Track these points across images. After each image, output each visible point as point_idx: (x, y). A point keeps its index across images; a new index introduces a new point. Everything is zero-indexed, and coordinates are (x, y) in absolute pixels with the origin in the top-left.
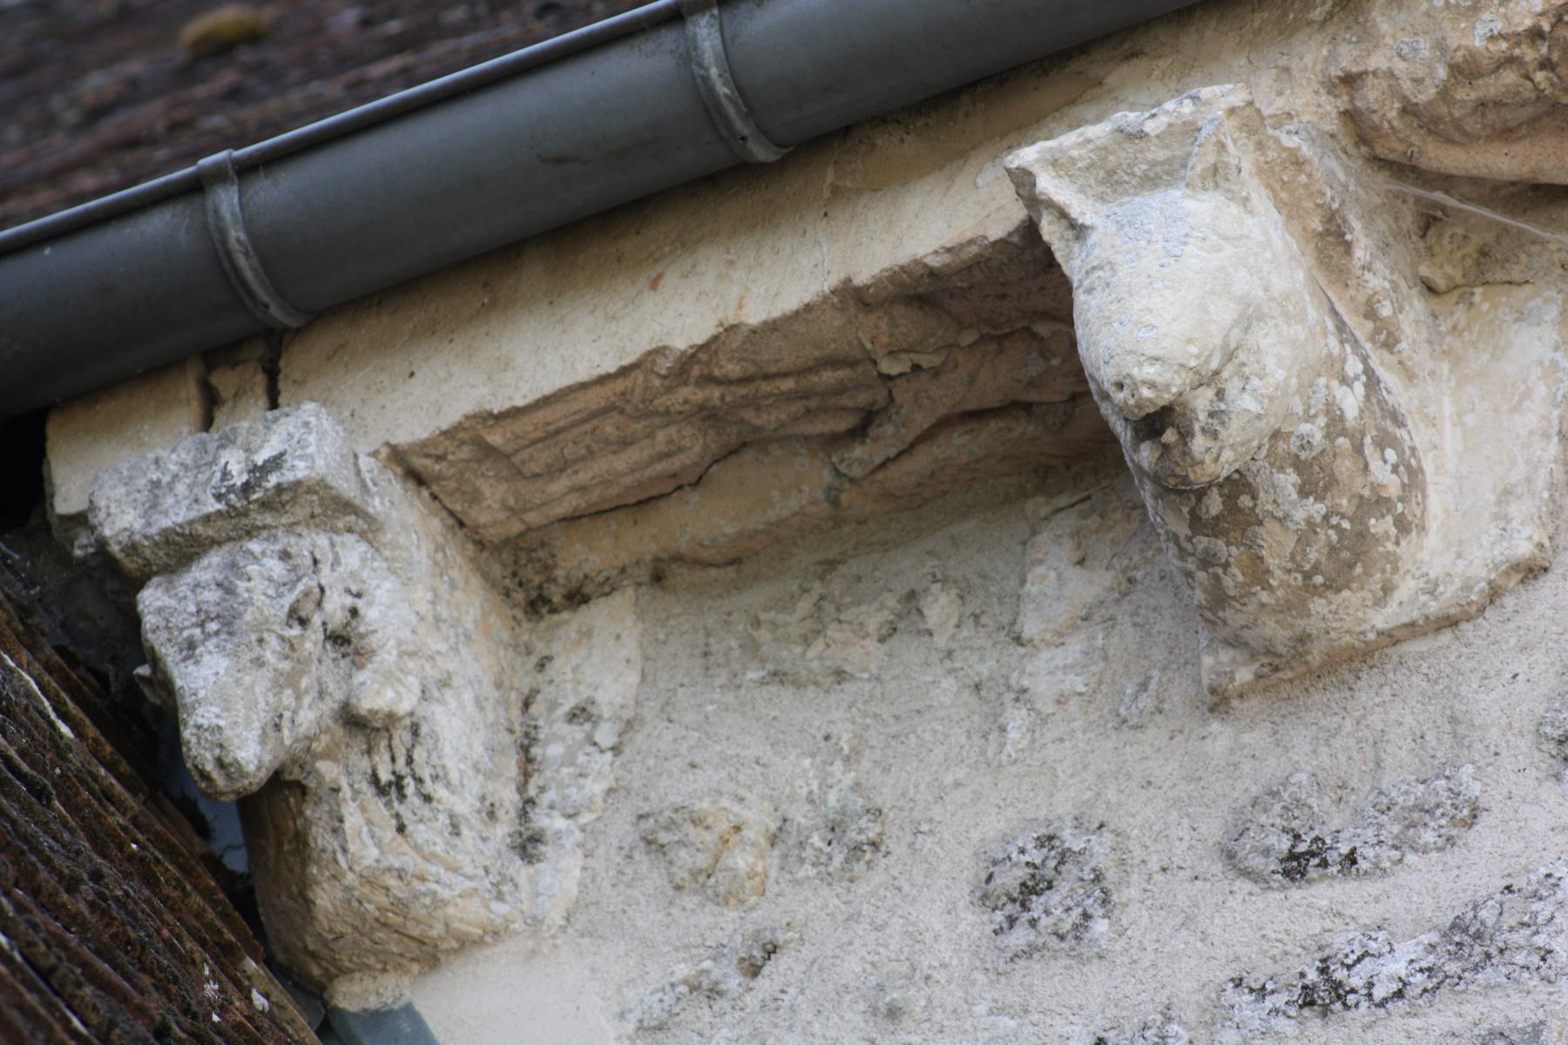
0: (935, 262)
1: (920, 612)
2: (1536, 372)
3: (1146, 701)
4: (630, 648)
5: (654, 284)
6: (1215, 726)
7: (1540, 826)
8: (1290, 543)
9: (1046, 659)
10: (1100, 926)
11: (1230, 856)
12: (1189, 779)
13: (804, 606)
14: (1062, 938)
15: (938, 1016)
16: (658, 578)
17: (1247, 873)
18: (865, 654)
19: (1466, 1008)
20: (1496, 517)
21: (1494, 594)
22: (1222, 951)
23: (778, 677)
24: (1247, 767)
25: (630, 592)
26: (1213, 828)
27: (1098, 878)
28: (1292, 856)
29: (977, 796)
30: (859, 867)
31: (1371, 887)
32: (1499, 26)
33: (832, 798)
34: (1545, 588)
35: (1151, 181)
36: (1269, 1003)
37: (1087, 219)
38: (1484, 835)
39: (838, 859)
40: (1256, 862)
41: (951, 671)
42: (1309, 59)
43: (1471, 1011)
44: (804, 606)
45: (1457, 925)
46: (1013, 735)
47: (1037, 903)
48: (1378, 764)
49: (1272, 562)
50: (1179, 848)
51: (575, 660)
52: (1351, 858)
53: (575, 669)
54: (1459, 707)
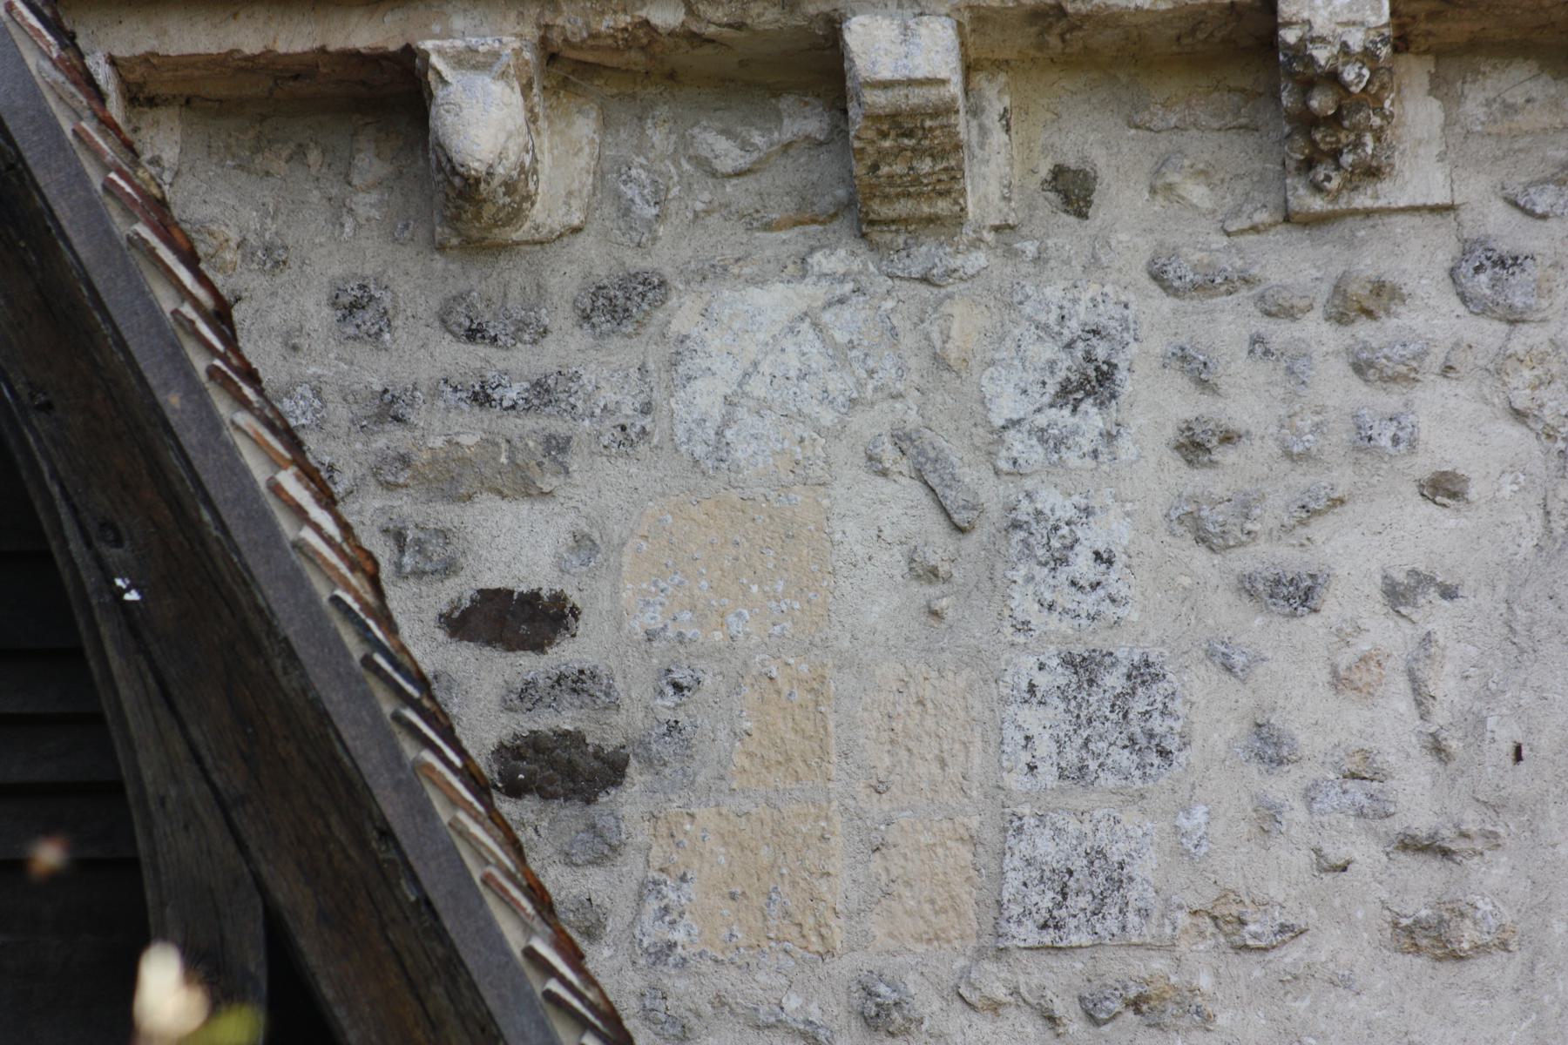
0: (363, 51)
1: (305, 155)
2: (585, 141)
3: (407, 234)
4: (177, 137)
5: (235, 16)
6: (437, 256)
7: (573, 347)
8: (494, 210)
9: (361, 198)
10: (387, 336)
11: (443, 321)
12: (425, 277)
13: (251, 133)
14: (370, 336)
15: (313, 354)
16: (188, 101)
17: (451, 332)
18: (279, 166)
19: (540, 421)
20: (565, 203)
21: (561, 236)
22: (439, 365)
23: (240, 167)
24: (451, 280)
25: (177, 108)
26: (435, 304)
27: (386, 312)
28: (470, 329)
29: (330, 253)
30: (277, 271)
31: (503, 354)
32: (612, 24)
33: (267, 236)
34: (581, 237)
35: (475, 67)
36: (459, 394)
37: (449, 79)
38: (550, 343)
39: (268, 265)
40: (456, 329)
41: (317, 188)
42: (532, 12)
43: (543, 422)
44: (251, 133)
45: (538, 383)
46: (347, 230)
47: (359, 314)
48: (505, 295)
49: (485, 215)
50: (421, 309)
51: (151, 134)
52: (495, 339)
53: (151, 138)
54: (542, 282)
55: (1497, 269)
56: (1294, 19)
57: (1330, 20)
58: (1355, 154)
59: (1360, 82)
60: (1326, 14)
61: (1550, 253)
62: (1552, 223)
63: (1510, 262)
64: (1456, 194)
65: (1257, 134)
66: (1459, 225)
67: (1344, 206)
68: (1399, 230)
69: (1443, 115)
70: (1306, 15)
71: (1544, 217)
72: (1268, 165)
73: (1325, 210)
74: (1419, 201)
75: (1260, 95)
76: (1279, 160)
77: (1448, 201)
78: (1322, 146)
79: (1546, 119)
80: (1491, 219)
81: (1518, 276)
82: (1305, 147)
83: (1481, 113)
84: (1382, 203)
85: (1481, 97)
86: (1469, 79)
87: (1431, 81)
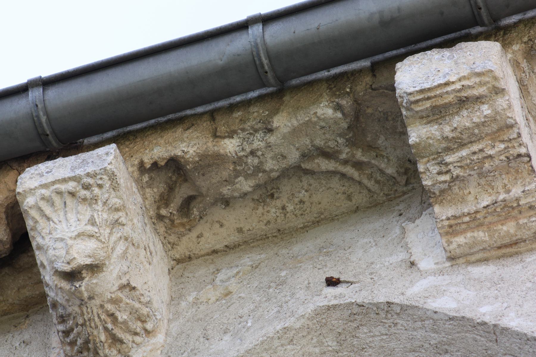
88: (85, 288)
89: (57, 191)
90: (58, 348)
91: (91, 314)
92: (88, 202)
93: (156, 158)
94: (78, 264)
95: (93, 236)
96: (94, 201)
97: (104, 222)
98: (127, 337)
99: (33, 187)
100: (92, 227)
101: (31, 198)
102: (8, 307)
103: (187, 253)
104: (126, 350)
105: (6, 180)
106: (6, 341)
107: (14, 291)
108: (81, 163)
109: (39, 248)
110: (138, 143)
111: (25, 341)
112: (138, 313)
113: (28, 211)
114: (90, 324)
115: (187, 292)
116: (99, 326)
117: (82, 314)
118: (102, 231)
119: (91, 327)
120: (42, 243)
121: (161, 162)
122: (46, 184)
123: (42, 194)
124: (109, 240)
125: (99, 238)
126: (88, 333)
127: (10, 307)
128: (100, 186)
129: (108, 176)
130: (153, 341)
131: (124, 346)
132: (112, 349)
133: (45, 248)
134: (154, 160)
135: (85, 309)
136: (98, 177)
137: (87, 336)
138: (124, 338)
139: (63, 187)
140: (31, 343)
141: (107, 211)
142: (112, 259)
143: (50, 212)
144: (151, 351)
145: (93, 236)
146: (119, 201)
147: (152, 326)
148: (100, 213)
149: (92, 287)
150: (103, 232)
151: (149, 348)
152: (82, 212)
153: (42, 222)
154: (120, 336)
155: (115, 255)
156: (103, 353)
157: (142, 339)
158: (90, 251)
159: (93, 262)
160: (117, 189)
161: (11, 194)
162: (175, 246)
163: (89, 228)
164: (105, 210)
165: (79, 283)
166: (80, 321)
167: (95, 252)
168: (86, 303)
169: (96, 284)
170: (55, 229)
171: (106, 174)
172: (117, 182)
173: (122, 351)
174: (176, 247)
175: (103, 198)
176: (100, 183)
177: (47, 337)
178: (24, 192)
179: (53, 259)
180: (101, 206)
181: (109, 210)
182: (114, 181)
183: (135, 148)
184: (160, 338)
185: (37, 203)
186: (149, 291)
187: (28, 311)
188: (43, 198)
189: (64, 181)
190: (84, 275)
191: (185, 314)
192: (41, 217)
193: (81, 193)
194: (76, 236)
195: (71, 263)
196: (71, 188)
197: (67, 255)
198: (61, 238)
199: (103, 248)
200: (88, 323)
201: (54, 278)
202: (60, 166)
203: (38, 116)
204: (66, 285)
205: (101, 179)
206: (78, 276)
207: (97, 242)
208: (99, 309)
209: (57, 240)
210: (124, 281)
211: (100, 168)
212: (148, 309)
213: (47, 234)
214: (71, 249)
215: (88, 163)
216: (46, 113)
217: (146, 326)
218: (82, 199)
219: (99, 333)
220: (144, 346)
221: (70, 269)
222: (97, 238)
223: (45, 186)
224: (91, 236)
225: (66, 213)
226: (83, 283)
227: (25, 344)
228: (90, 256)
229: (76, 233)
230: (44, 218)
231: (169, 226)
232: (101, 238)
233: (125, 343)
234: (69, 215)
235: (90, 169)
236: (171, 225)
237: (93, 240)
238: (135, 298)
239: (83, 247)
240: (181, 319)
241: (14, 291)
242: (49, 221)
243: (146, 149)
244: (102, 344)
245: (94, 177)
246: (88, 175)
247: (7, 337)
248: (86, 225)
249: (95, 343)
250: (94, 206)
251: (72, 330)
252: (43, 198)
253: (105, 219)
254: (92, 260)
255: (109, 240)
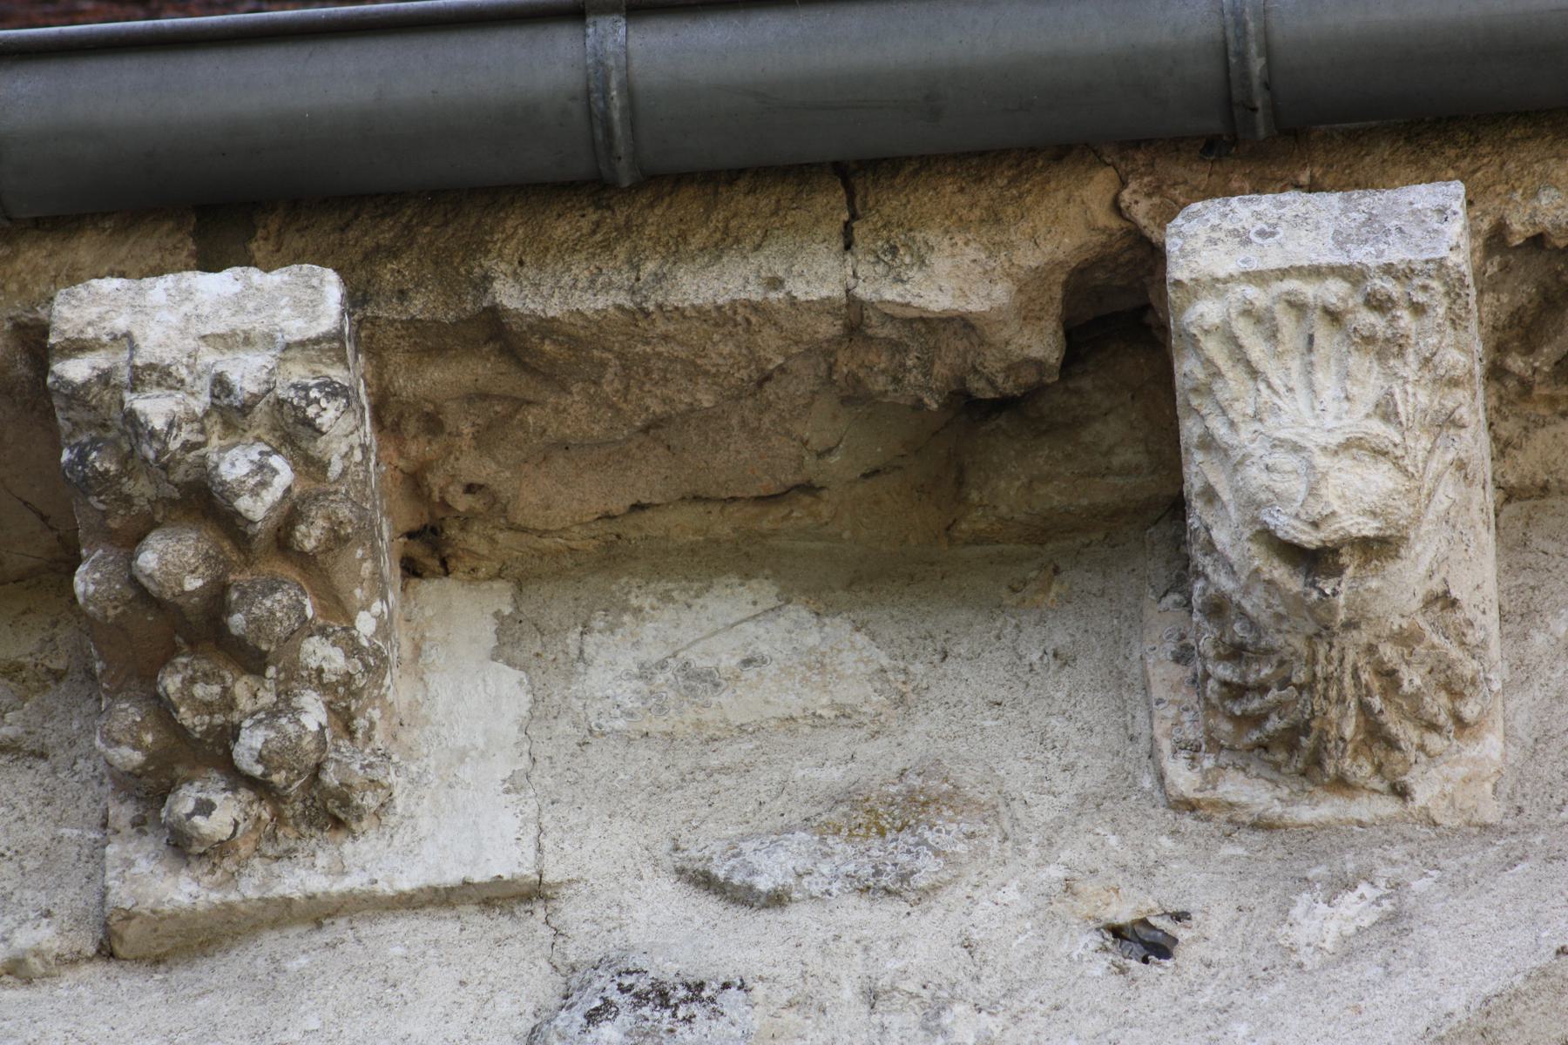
55: (646, 1011)
56: (90, 333)
57: (183, 332)
58: (270, 727)
59: (264, 484)
60: (174, 319)
61: (788, 975)
62: (798, 915)
63: (682, 993)
64: (550, 860)
65: (43, 766)
66: (557, 933)
67: (252, 894)
68: (398, 951)
69: (526, 699)
70: (121, 323)
71: (777, 900)
72: (66, 832)
73: (201, 906)
74: (452, 876)
75: (58, 676)
76: (96, 818)
77: (528, 872)
78: (186, 716)
79: (791, 700)
80: (641, 914)
81: (701, 1024)
82: (142, 726)
83: (627, 693)
84: (354, 882)
85: (628, 660)
86: (598, 624)
87: (499, 633)
88: (1347, 599)
89: (1293, 298)
90: (1170, 702)
91: (1336, 664)
92: (1377, 348)
93: (1546, 222)
94: (1341, 533)
95: (1385, 454)
96: (1396, 349)
97: (1418, 416)
98: (1407, 733)
99: (1221, 274)
100: (1383, 427)
101: (1210, 304)
102: (992, 524)
103: (1542, 476)
104: (1399, 768)
105: (1084, 193)
106: (998, 637)
107: (1018, 484)
108: (1364, 224)
109: (1208, 443)
110: (1486, 160)
111: (1061, 651)
112: (1449, 673)
113: (1198, 341)
114: (1326, 690)
115: (1547, 604)
116: (1349, 697)
117: (1313, 660)
118: (1410, 443)
119: (1326, 697)
120: (1226, 439)
121: (1560, 238)
122: (1260, 272)
123: (1246, 301)
124: (1424, 468)
125: (1400, 462)
126: (1313, 711)
127: (997, 526)
128: (1418, 309)
129: (1446, 283)
130: (1472, 751)
131: (1397, 755)
132: (1362, 760)
133: (1236, 455)
134: (1538, 230)
135: (1322, 651)
136: (1417, 281)
137: (1307, 717)
138: (1402, 736)
139: (1309, 291)
140: (1074, 660)
141: (1430, 385)
142: (1424, 524)
143: (1262, 355)
144: (1467, 781)
145: (1385, 454)
146: (1463, 359)
147: (1477, 709)
148: (1409, 388)
149: (1364, 600)
150: (1412, 445)
151: (1462, 771)
152: (1360, 376)
153: (1234, 378)
154: (1394, 731)
155: (1431, 516)
156: (1336, 767)
157: (1446, 743)
158: (1375, 498)
159: (1381, 529)
160: (1464, 324)
161: (1094, 239)
162: (1509, 449)
163: (1377, 427)
164: (1423, 382)
165: (1333, 581)
166: (1301, 676)
167: (1390, 502)
168: (1334, 634)
169: (1378, 591)
170: (1276, 410)
171: (1439, 278)
172: (1467, 304)
173: (1386, 769)
174: (1515, 452)
175: (1422, 344)
176: (1421, 300)
177: (1122, 652)
178: (1193, 283)
179: (1263, 496)
180: (1415, 366)
181: (1434, 381)
182: (1459, 301)
183: (1479, 174)
184: (1491, 747)
185: (1227, 323)
186: (1484, 613)
187: (1042, 544)
188: (1247, 312)
189: (1316, 272)
190: (1344, 560)
191: (1548, 673)
192: (1230, 363)
193: (1358, 316)
194: (1340, 445)
195: (1323, 527)
196: (1334, 300)
197: (1311, 500)
198: (1296, 443)
199: (1408, 491)
200: (1319, 687)
201: (1254, 548)
202: (1300, 220)
203: (1243, 56)
204: (1286, 576)
205: (1425, 288)
206: (1327, 560)
207: (1394, 473)
208: (1362, 656)
209: (1278, 444)
210: (1436, 586)
211: (1426, 256)
212: (1475, 663)
213: (1247, 419)
214: (1323, 483)
215: (1387, 233)
216: (1267, 50)
217: (1462, 709)
218: (1363, 337)
219: (1343, 715)
220: (1446, 762)
221: (1319, 544)
222: (1396, 462)
223: (1258, 278)
224: (1380, 453)
225: (1309, 369)
226: (1343, 585)
227: (1059, 662)
228: (1374, 514)
229: (1338, 438)
230: (1240, 367)
231: (1512, 397)
232: (1407, 461)
233: (1400, 749)
234: (1319, 377)
235: (1397, 254)
236: (1520, 395)
237: (1385, 466)
238: (1452, 632)
239: (1359, 484)
240: (1536, 686)
241: (1018, 484)
242: (1255, 379)
243: (1514, 189)
244: (1341, 745)
245: (1403, 278)
246: (1388, 270)
247: (998, 624)
248: (1368, 416)
249: (1322, 739)
250: (1392, 362)
251: (1263, 689)
252: (1247, 312)
253: (1423, 407)
254: (1379, 525)
255: (1424, 468)
